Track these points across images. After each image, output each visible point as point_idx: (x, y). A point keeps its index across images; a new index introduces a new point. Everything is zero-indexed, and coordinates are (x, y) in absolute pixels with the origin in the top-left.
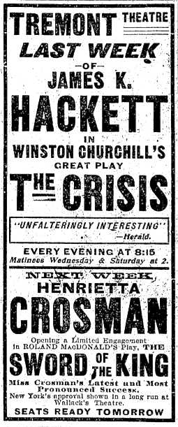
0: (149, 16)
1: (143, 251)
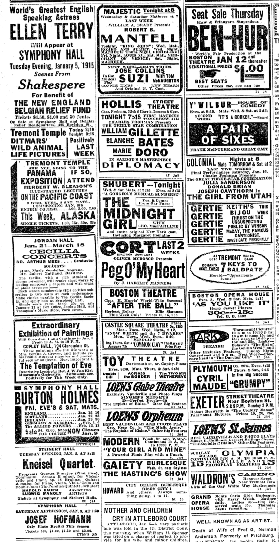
0: (162, 292)
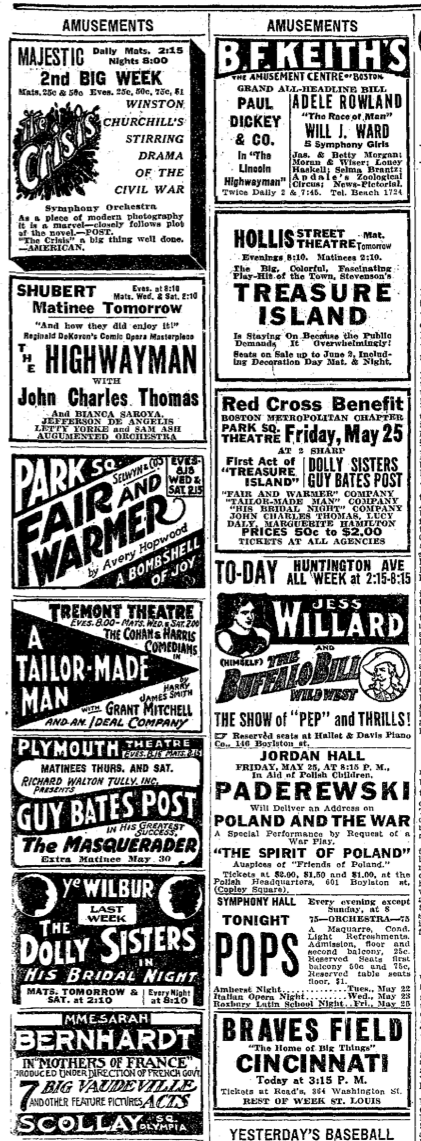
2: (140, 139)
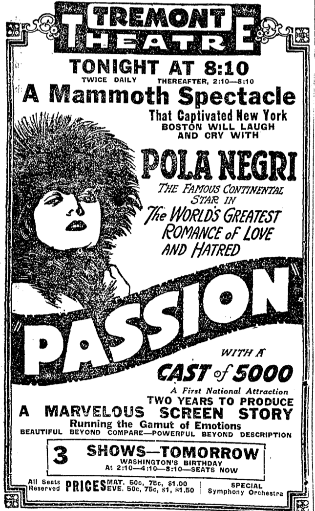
1: (220, 67)
2: (45, 432)
